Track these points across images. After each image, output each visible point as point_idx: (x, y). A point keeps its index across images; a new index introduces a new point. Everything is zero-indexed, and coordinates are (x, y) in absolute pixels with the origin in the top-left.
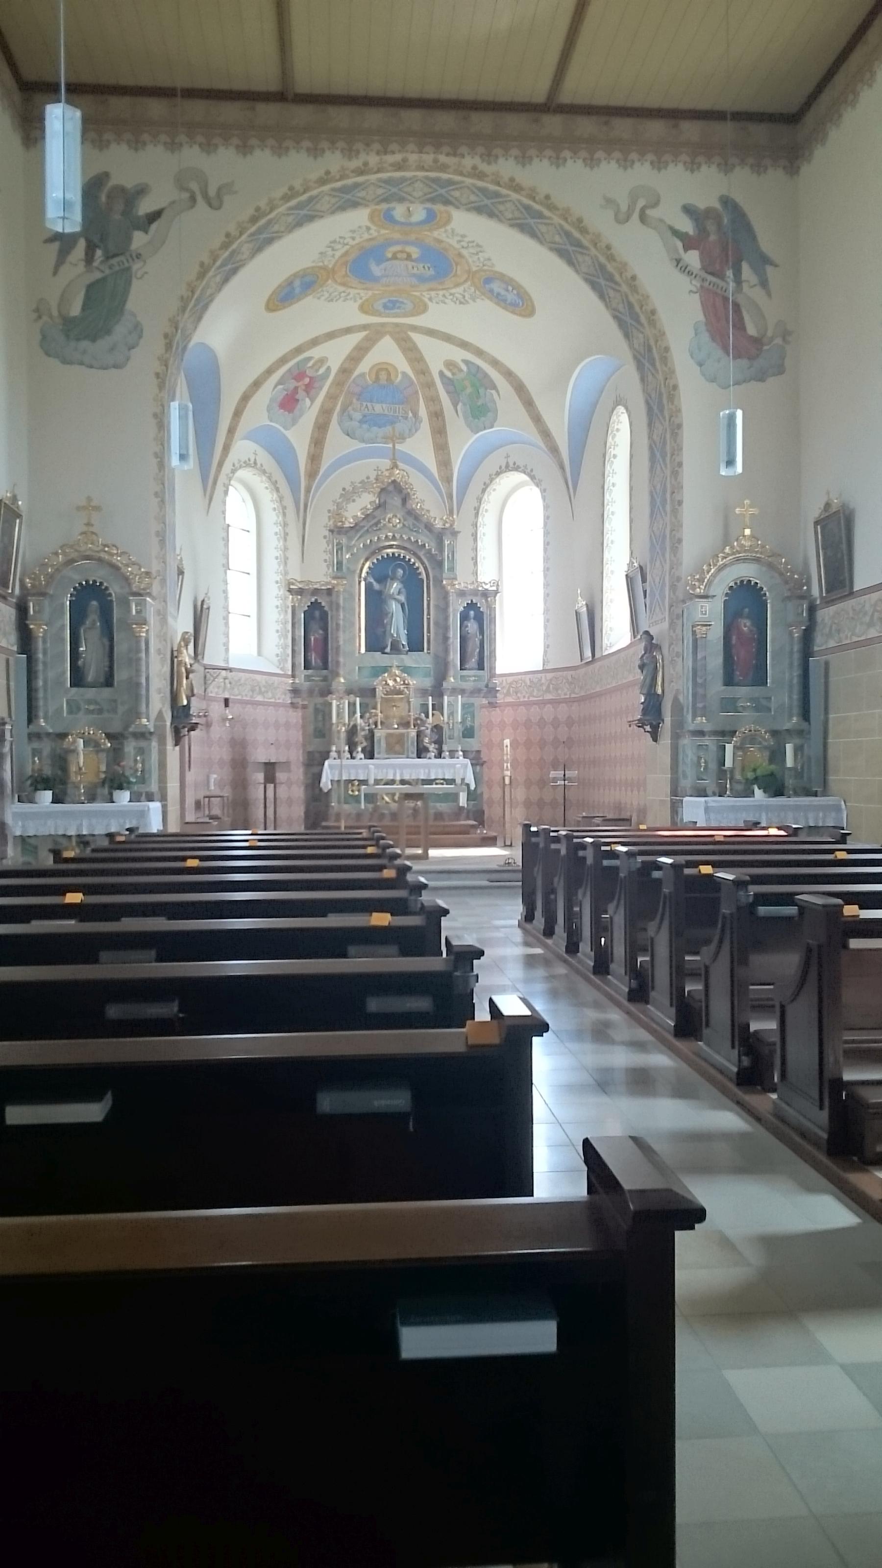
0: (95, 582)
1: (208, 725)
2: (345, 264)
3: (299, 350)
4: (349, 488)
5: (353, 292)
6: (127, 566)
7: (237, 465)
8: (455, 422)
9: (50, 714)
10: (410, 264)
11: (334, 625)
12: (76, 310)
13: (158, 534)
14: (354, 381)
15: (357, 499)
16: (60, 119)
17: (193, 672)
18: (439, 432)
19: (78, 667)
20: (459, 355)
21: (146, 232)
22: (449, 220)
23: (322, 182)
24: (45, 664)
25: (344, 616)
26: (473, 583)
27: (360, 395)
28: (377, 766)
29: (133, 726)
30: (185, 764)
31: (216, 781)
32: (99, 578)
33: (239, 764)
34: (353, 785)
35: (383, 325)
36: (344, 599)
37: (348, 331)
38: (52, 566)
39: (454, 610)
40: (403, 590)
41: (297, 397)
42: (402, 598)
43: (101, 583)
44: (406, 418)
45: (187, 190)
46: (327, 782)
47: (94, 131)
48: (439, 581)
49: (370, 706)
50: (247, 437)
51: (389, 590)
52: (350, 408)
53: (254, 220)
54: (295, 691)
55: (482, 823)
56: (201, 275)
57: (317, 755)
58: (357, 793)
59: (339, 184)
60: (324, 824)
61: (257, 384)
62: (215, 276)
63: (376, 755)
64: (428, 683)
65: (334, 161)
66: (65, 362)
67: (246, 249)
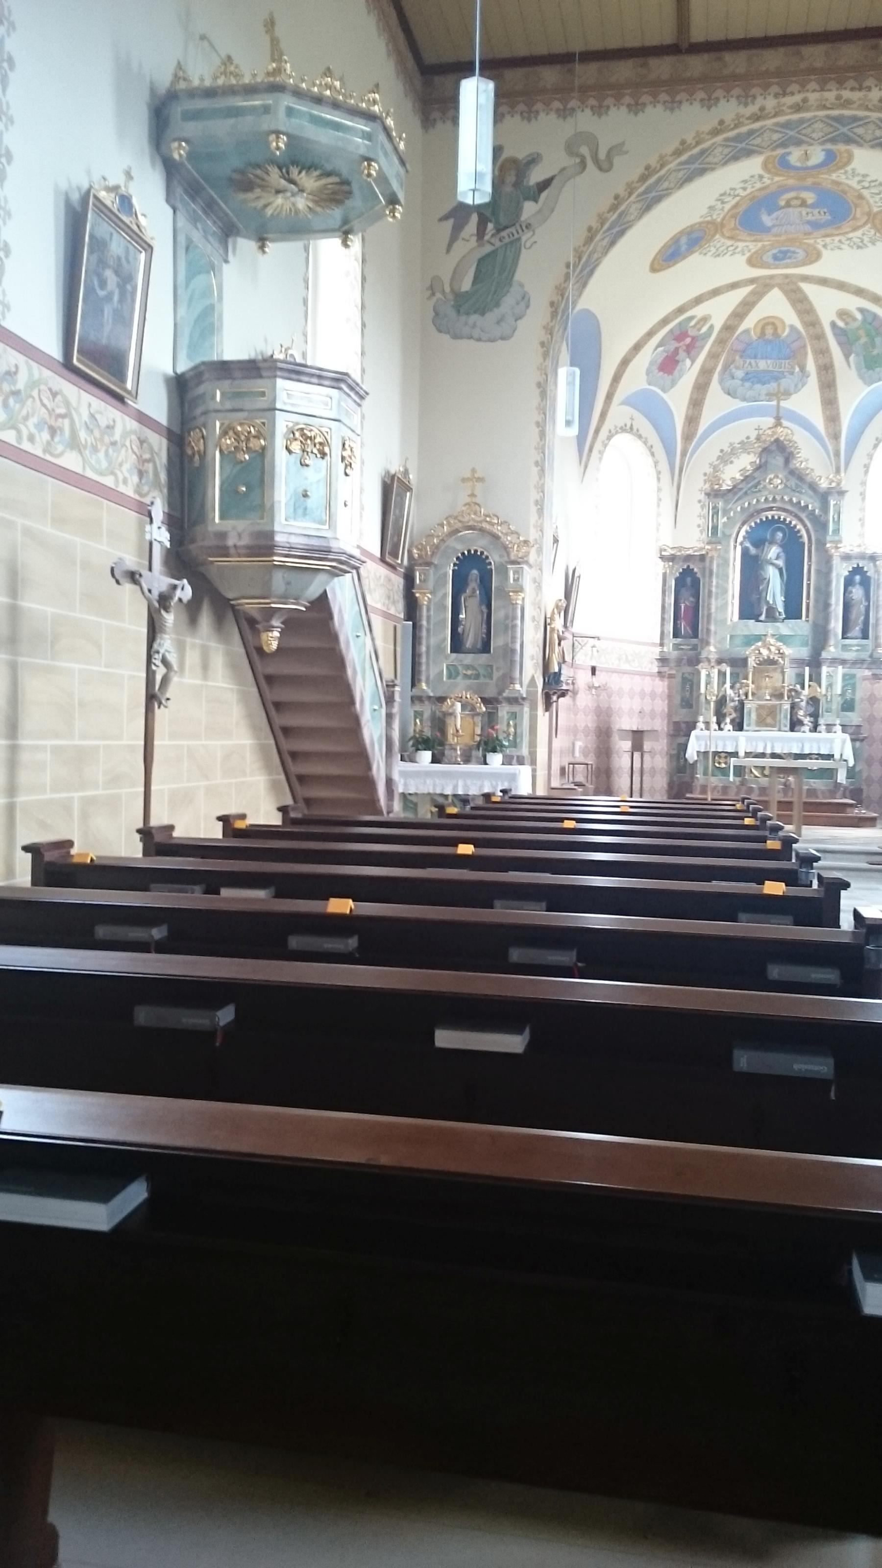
0: (476, 551)
1: (575, 693)
2: (734, 216)
3: (681, 310)
4: (727, 449)
5: (741, 245)
6: (506, 534)
7: (613, 431)
8: (846, 374)
9: (432, 677)
10: (804, 211)
11: (706, 591)
12: (466, 285)
13: (537, 503)
14: (737, 338)
15: (735, 460)
16: (475, 95)
17: (564, 639)
18: (828, 386)
19: (459, 634)
20: (852, 303)
21: (536, 201)
22: (850, 158)
23: (715, 132)
24: (428, 630)
25: (717, 583)
26: (860, 546)
27: (744, 352)
28: (748, 739)
29: (507, 691)
30: (554, 730)
31: (581, 748)
33: (603, 735)
34: (720, 757)
35: (772, 277)
36: (718, 566)
37: (734, 286)
38: (438, 536)
39: (838, 575)
40: (782, 554)
42: (781, 563)
43: (482, 553)
44: (792, 373)
45: (578, 155)
46: (692, 753)
47: (505, 103)
48: (821, 544)
49: (741, 676)
50: (623, 403)
51: (767, 554)
52: (732, 366)
53: (643, 178)
54: (663, 660)
55: (860, 803)
56: (589, 240)
57: (683, 726)
58: (723, 765)
59: (731, 134)
60: (688, 795)
61: (637, 348)
62: (603, 239)
63: (745, 727)
64: (804, 652)
65: (728, 109)
66: (456, 337)
67: (634, 210)
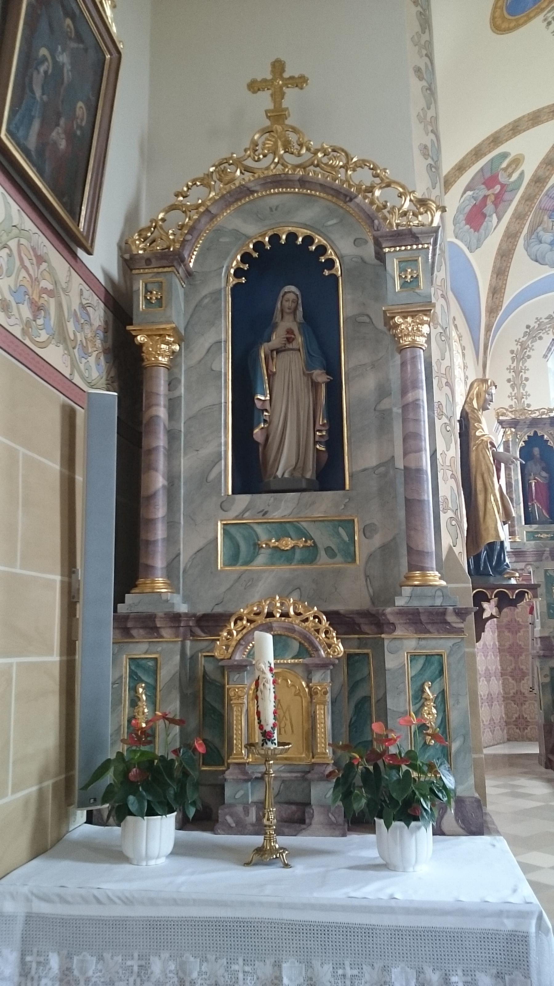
0: (292, 236)
13: (425, 151)
14: (546, 194)
24: (172, 436)
29: (407, 591)
32: (305, 226)
41: (485, 211)
